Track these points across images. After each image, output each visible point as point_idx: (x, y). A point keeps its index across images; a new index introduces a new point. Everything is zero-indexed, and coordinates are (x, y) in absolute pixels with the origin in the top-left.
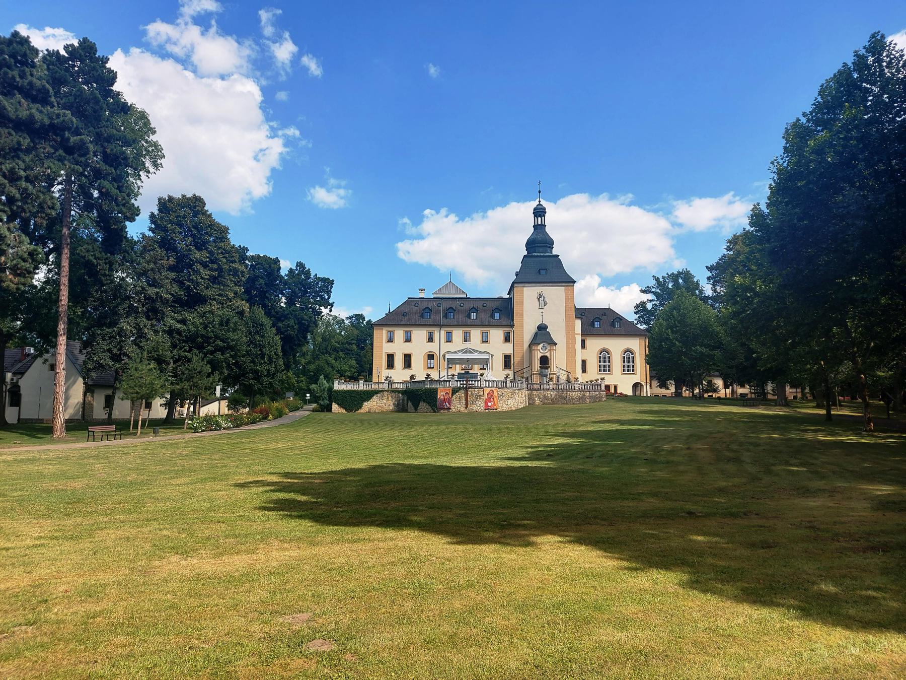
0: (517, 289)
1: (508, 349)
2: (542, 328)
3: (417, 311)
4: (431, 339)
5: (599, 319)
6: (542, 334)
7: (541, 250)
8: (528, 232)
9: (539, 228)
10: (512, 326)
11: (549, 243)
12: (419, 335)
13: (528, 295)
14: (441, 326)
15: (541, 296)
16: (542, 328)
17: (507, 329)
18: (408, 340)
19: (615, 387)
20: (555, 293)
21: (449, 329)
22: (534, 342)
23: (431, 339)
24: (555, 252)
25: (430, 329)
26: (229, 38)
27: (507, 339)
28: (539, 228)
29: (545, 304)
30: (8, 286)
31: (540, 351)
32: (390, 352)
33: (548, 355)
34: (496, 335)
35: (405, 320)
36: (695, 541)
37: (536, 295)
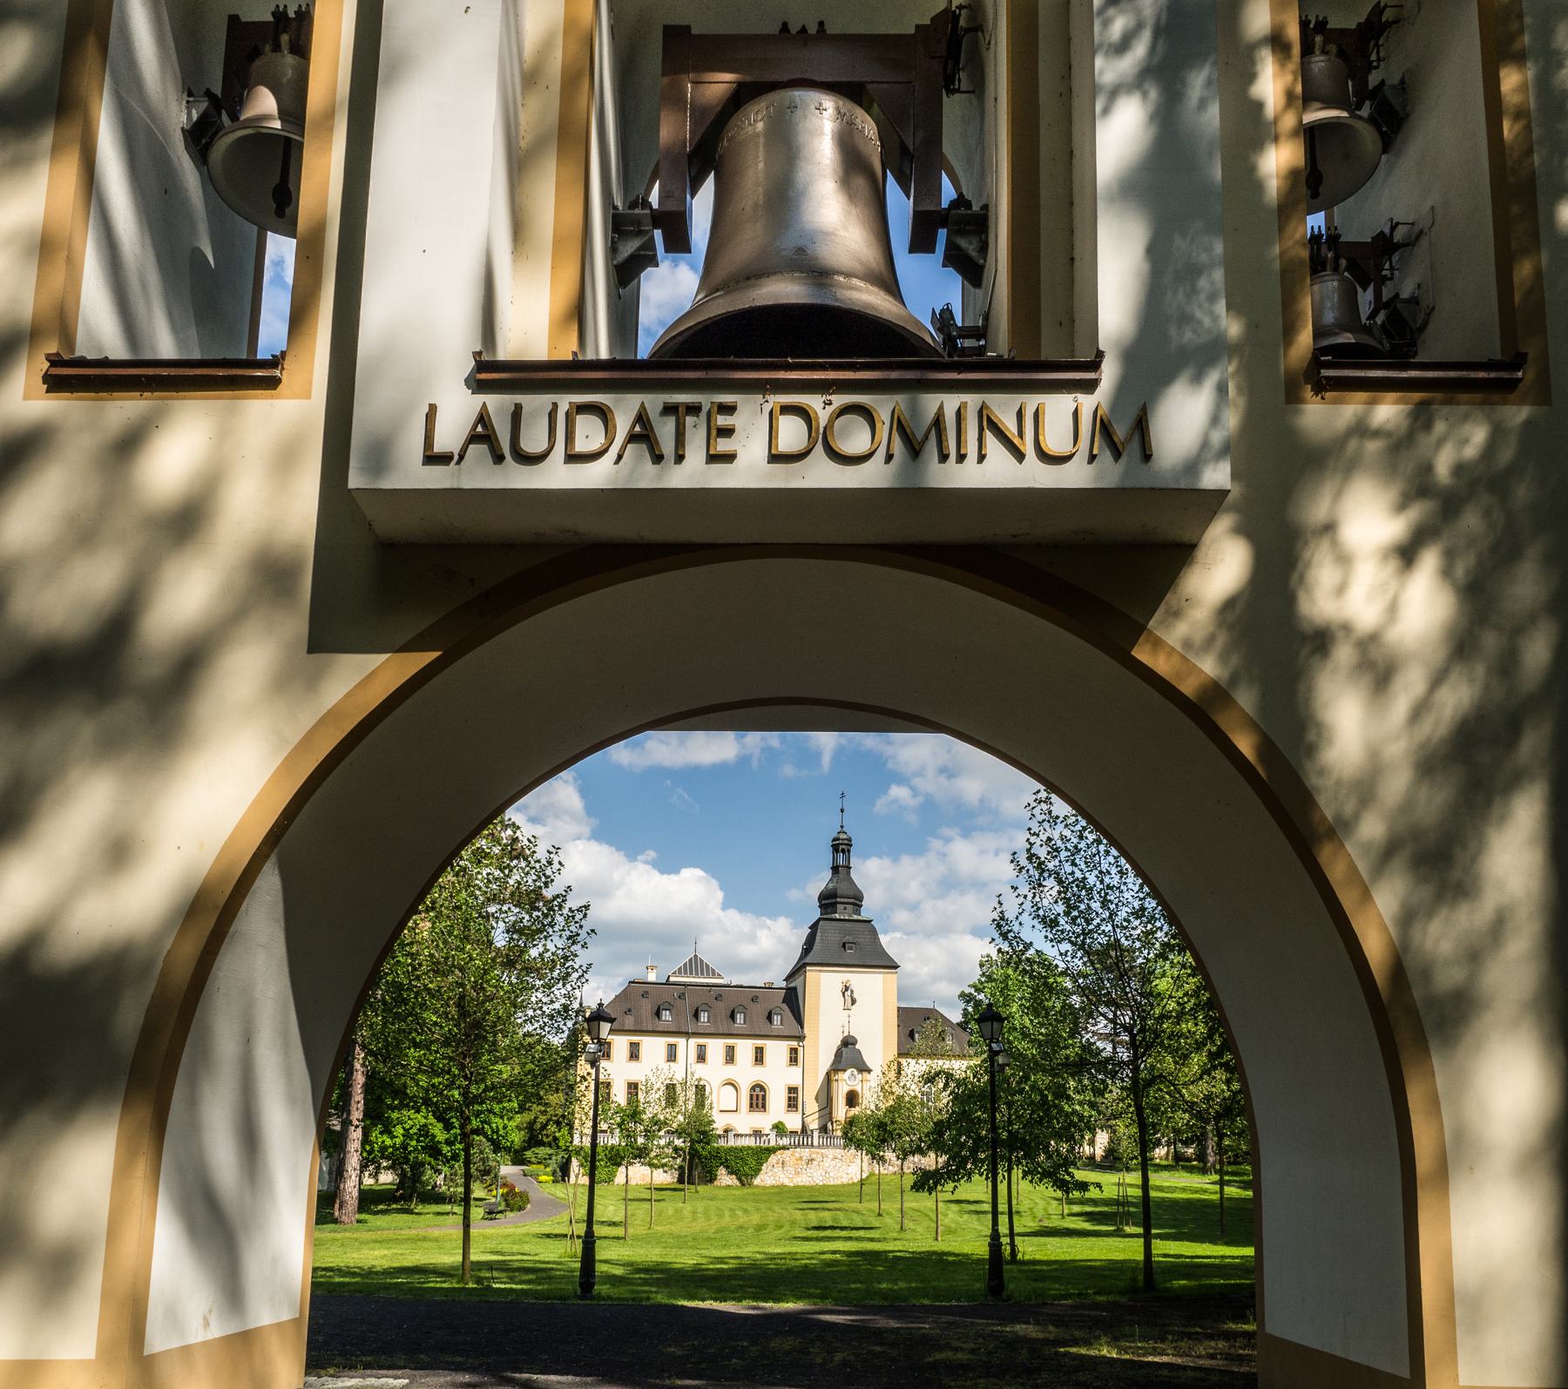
0: (812, 974)
1: (793, 1076)
2: (849, 1042)
3: (647, 1007)
4: (672, 1056)
5: (744, 1010)
6: (848, 1055)
8: (821, 880)
10: (800, 1038)
11: (857, 900)
12: (654, 1047)
13: (824, 985)
14: (687, 1035)
15: (847, 988)
16: (849, 1042)
17: (794, 1044)
18: (634, 1054)
20: (872, 986)
21: (702, 1041)
22: (838, 1065)
23: (672, 1056)
24: (864, 915)
25: (672, 1040)
26: (1307, 554)
27: (794, 1060)
29: (854, 1002)
30: (405, 1086)
31: (846, 1081)
34: (777, 1050)
35: (629, 1022)
36: (798, 1298)
37: (840, 987)
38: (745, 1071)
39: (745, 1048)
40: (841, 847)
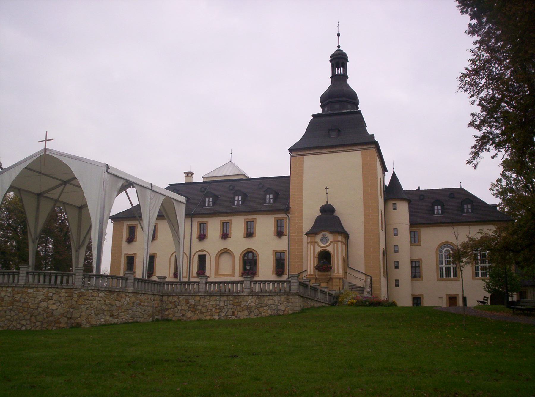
1: (282, 244)
2: (327, 210)
6: (328, 220)
7: (337, 106)
8: (324, 83)
9: (339, 79)
10: (287, 210)
11: (352, 99)
19: (465, 299)
20: (352, 160)
21: (202, 220)
28: (339, 79)
32: (130, 252)
33: (330, 249)
34: (265, 225)
38: (238, 243)
39: (238, 225)
40: (339, 60)
